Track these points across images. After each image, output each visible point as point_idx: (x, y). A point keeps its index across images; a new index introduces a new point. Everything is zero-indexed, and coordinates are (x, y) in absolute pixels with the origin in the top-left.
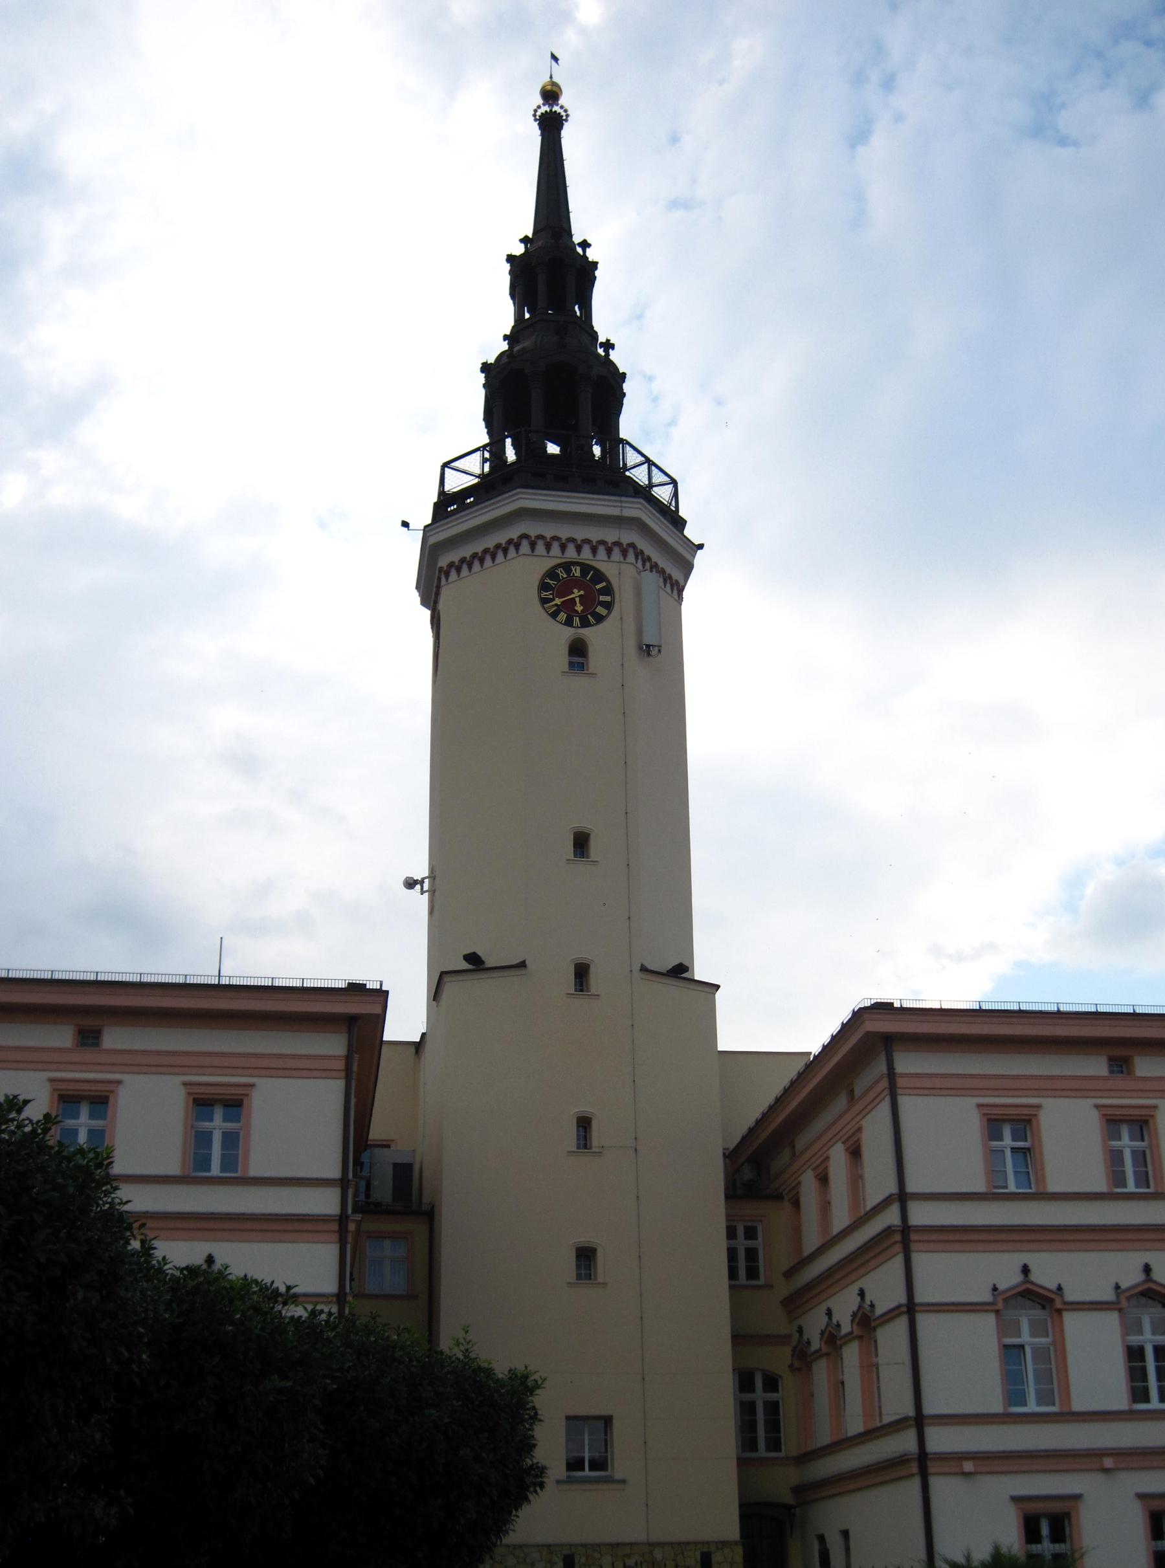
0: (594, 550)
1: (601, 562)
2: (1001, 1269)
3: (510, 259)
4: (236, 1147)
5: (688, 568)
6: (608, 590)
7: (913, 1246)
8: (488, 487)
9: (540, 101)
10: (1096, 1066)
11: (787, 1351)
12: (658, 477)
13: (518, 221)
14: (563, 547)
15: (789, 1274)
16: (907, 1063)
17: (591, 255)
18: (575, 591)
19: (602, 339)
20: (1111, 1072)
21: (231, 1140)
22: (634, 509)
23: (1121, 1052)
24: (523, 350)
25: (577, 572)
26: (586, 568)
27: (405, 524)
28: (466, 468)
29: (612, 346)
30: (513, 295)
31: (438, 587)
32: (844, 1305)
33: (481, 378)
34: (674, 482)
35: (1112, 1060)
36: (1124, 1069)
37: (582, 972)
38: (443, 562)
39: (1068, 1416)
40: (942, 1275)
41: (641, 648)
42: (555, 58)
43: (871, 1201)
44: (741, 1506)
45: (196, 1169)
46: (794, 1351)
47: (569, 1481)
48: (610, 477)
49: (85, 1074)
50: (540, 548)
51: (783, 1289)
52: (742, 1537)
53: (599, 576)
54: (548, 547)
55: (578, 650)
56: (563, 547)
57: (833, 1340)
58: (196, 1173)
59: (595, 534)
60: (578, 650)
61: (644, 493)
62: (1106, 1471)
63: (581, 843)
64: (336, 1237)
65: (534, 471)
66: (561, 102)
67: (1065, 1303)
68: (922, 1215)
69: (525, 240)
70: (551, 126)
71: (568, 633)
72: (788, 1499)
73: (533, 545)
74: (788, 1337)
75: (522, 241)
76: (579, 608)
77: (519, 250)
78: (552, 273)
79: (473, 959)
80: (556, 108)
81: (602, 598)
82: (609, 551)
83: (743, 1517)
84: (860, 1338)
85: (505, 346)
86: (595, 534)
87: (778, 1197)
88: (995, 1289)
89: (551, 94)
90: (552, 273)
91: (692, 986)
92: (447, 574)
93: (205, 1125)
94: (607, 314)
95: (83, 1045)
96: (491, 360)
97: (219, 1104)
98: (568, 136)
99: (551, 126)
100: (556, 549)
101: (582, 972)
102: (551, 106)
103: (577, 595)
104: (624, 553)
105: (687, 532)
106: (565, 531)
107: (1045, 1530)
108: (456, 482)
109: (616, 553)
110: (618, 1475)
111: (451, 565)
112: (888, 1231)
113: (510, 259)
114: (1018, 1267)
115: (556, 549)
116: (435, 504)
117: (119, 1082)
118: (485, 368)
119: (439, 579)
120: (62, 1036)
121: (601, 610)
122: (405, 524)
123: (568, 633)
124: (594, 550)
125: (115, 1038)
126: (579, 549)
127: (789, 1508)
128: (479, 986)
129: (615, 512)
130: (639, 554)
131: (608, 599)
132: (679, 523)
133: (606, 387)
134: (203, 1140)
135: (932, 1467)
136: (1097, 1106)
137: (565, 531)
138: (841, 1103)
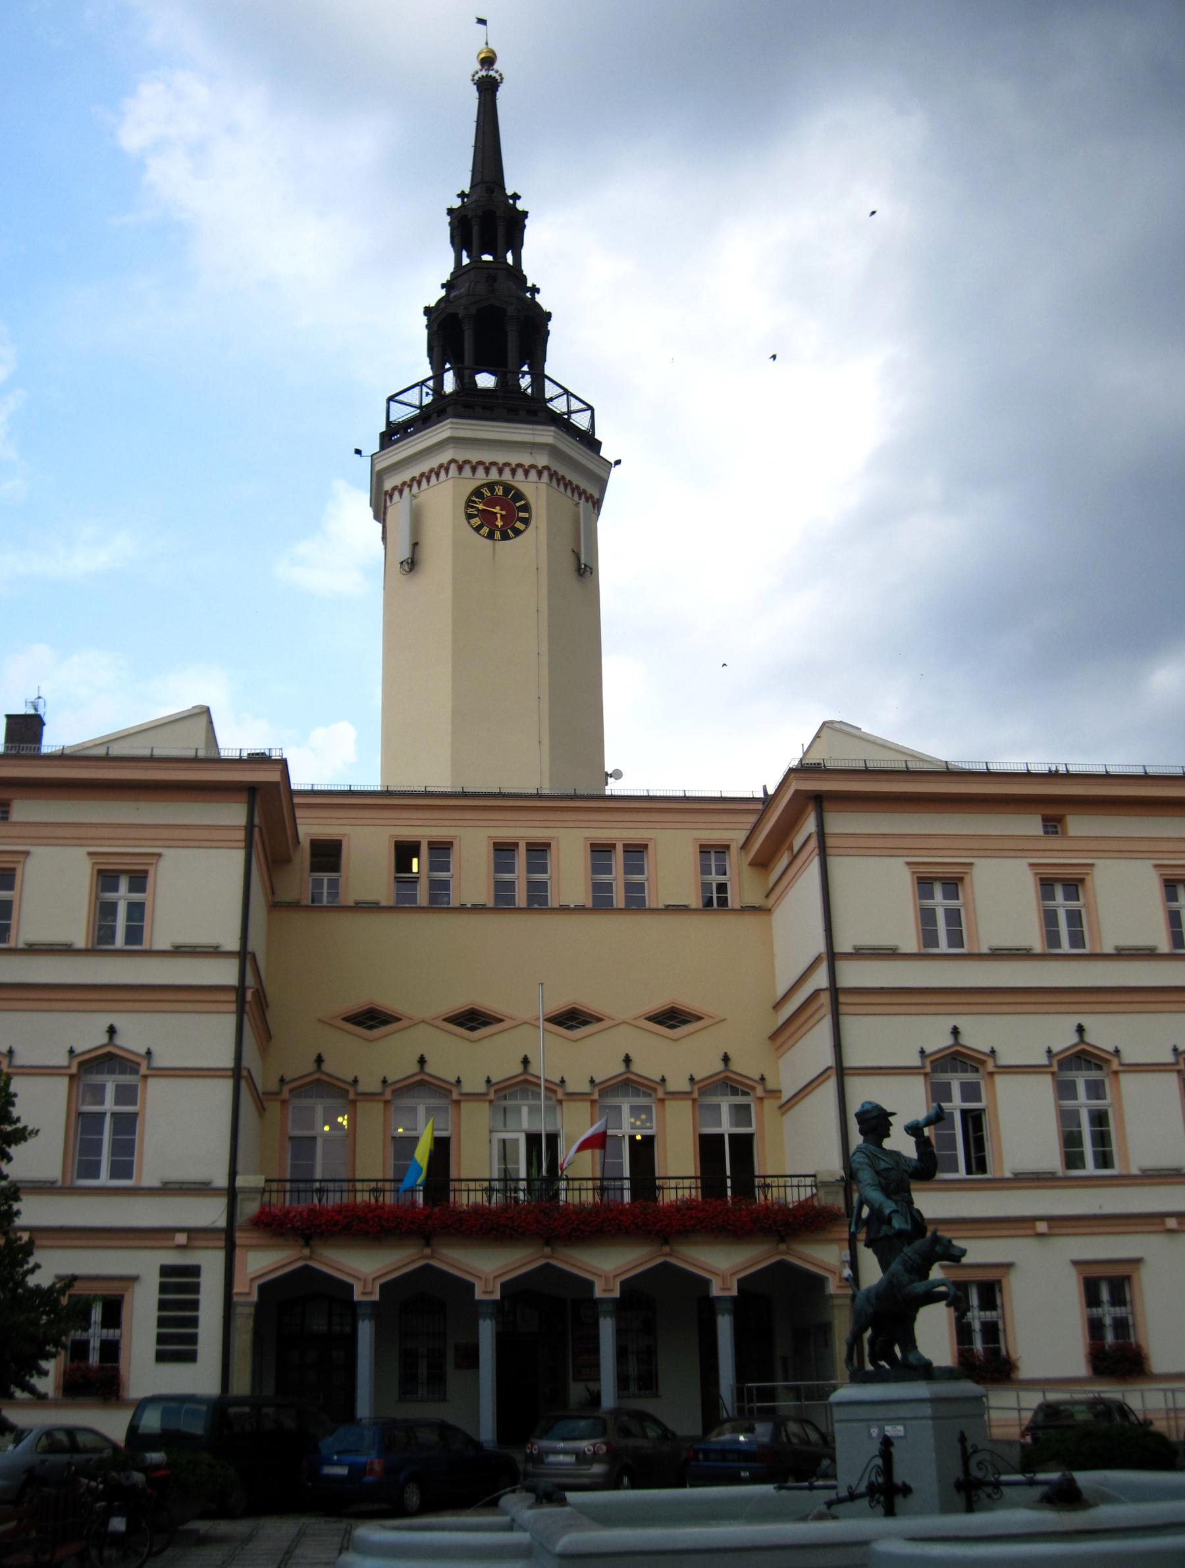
0: (513, 472)
2: (1058, 1032)
3: (450, 211)
4: (141, 918)
6: (526, 508)
7: (843, 1009)
8: (426, 418)
9: (479, 67)
10: (1030, 825)
13: (459, 178)
14: (487, 470)
16: (840, 823)
17: (520, 205)
18: (498, 508)
19: (529, 284)
20: (1046, 832)
21: (137, 911)
22: (547, 435)
24: (457, 298)
25: (499, 491)
26: (508, 488)
27: (358, 452)
28: (406, 400)
29: (538, 291)
31: (385, 507)
33: (424, 320)
34: (590, 408)
35: (1046, 820)
36: (1059, 829)
38: (388, 485)
39: (1001, 1183)
48: (534, 408)
50: (467, 470)
53: (519, 496)
54: (474, 469)
56: (487, 470)
58: (101, 942)
61: (562, 422)
62: (1170, 1231)
65: (469, 404)
66: (496, 67)
67: (1121, 1065)
68: (853, 975)
69: (462, 195)
70: (488, 88)
75: (459, 196)
76: (499, 523)
77: (457, 203)
78: (488, 222)
80: (492, 73)
81: (521, 515)
82: (526, 473)
85: (443, 293)
89: (488, 61)
90: (488, 222)
92: (391, 497)
93: (110, 896)
94: (543, 258)
96: (433, 305)
98: (503, 97)
99: (488, 88)
100: (480, 471)
102: (488, 70)
103: (497, 511)
105: (603, 453)
106: (487, 457)
107: (1105, 1295)
108: (401, 413)
111: (395, 488)
112: (816, 993)
113: (450, 211)
114: (949, 1028)
115: (480, 471)
116: (382, 435)
118: (428, 311)
121: (519, 525)
122: (358, 452)
124: (513, 472)
126: (501, 471)
131: (526, 515)
133: (531, 328)
134: (107, 910)
136: (908, 864)
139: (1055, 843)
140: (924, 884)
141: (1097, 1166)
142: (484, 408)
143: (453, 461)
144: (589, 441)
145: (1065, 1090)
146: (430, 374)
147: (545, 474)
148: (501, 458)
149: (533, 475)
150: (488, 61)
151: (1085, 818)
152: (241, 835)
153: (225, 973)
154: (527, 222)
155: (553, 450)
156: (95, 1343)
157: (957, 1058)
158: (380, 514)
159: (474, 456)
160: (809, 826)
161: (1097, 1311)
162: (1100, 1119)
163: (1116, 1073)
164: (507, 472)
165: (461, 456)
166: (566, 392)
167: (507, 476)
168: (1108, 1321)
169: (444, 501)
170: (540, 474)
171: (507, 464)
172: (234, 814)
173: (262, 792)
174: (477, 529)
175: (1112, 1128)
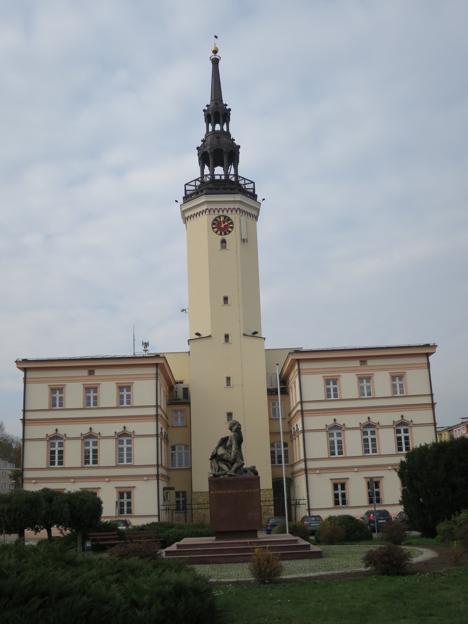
0: (227, 211)
1: (230, 215)
2: (328, 420)
3: (204, 111)
6: (232, 223)
7: (304, 415)
8: (198, 192)
10: (357, 363)
14: (218, 211)
16: (304, 366)
22: (238, 197)
26: (225, 217)
35: (361, 361)
37: (227, 337)
38: (186, 216)
39: (65, 468)
40: (313, 422)
44: (273, 479)
45: (120, 404)
49: (91, 382)
53: (229, 219)
54: (214, 212)
55: (224, 241)
56: (218, 211)
59: (227, 206)
60: (224, 241)
61: (244, 192)
63: (226, 299)
68: (307, 407)
69: (208, 106)
70: (215, 62)
71: (221, 237)
73: (210, 212)
75: (206, 106)
78: (218, 113)
79: (198, 334)
80: (217, 57)
81: (230, 226)
86: (227, 206)
88: (326, 425)
90: (218, 113)
91: (260, 339)
94: (238, 129)
97: (124, 388)
99: (215, 62)
101: (227, 337)
103: (222, 226)
106: (218, 206)
109: (234, 211)
111: (188, 217)
112: (298, 411)
113: (204, 111)
116: (184, 198)
118: (198, 148)
120: (85, 373)
121: (230, 229)
122: (176, 201)
123: (221, 237)
124: (227, 211)
125: (370, 363)
126: (223, 211)
129: (232, 199)
131: (232, 225)
135: (308, 472)
137: (218, 206)
139: (91, 377)
141: (373, 453)
143: (207, 209)
144: (253, 196)
146: (200, 176)
147: (238, 210)
148: (223, 206)
150: (215, 52)
151: (372, 360)
152: (155, 376)
153: (153, 412)
154: (231, 112)
155: (240, 202)
156: (125, 503)
157: (335, 427)
158: (185, 223)
159: (214, 206)
160: (296, 367)
161: (336, 492)
164: (225, 211)
165: (210, 207)
167: (225, 213)
169: (204, 222)
170: (236, 211)
172: (153, 371)
173: (157, 364)
174: (216, 232)
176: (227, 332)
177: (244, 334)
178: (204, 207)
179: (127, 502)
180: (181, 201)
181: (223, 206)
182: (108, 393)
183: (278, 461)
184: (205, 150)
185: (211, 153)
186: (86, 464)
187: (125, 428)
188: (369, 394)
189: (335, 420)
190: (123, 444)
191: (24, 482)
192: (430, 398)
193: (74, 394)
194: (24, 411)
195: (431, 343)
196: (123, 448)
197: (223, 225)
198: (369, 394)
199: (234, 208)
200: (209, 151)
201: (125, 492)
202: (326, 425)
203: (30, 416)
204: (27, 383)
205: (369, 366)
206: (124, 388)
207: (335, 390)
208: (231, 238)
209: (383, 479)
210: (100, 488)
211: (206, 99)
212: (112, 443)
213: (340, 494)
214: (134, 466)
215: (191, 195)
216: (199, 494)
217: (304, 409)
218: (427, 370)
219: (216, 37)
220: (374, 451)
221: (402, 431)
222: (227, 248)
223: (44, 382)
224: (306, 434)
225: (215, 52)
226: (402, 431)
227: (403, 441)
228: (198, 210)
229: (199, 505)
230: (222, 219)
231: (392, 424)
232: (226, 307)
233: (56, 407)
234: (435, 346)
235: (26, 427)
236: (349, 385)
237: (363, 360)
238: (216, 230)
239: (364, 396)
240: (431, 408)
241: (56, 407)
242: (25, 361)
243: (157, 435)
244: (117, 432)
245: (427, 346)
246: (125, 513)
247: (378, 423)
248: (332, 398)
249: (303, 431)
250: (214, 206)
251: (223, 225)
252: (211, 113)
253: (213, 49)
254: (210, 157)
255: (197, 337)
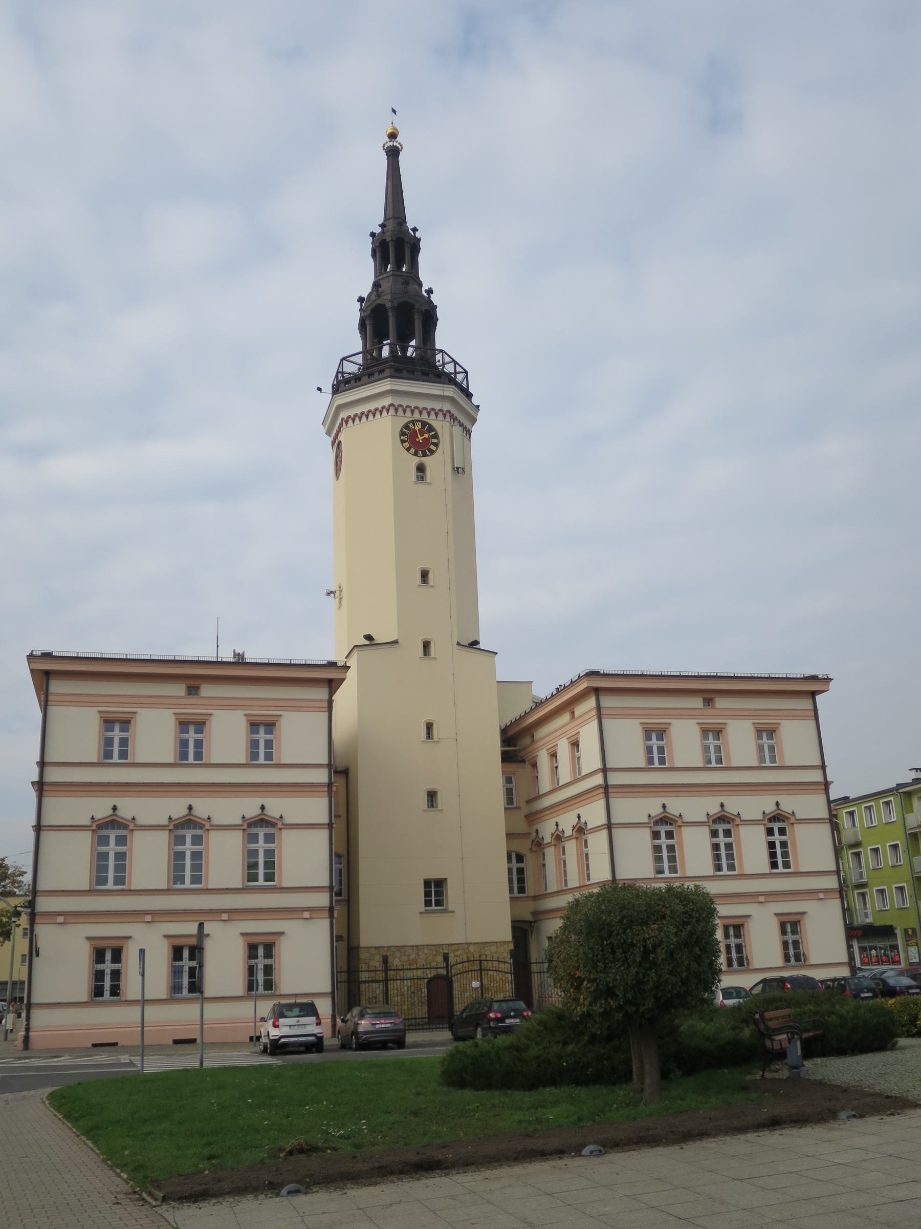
0: (429, 414)
3: (373, 235)
5: (473, 421)
6: (436, 436)
7: (610, 795)
10: (697, 703)
11: (529, 842)
12: (459, 369)
14: (412, 412)
15: (529, 802)
16: (608, 702)
17: (418, 235)
22: (450, 391)
23: (708, 696)
26: (424, 424)
30: (374, 255)
32: (567, 822)
34: (466, 372)
35: (704, 699)
37: (426, 645)
39: (743, 876)
41: (454, 469)
42: (394, 111)
43: (585, 772)
46: (533, 841)
47: (427, 912)
49: (192, 709)
51: (525, 810)
52: (513, 938)
53: (431, 429)
54: (404, 411)
55: (421, 469)
56: (412, 412)
57: (559, 838)
59: (429, 405)
60: (421, 469)
61: (450, 380)
63: (425, 575)
64: (326, 794)
68: (615, 779)
70: (393, 154)
72: (530, 918)
73: (396, 410)
74: (530, 834)
78: (396, 247)
79: (369, 637)
80: (395, 144)
81: (433, 441)
82: (437, 414)
83: (514, 928)
84: (577, 838)
86: (429, 405)
87: (523, 761)
88: (649, 816)
90: (396, 247)
94: (431, 272)
95: (189, 694)
97: (262, 726)
99: (393, 154)
101: (426, 645)
103: (418, 440)
104: (445, 416)
105: (473, 399)
106: (413, 403)
107: (789, 929)
110: (450, 909)
117: (211, 715)
119: (341, 424)
120: (179, 690)
122: (319, 389)
123: (416, 460)
124: (429, 414)
125: (207, 690)
126: (421, 413)
127: (530, 922)
128: (373, 654)
130: (452, 416)
131: (435, 441)
132: (469, 395)
137: (413, 403)
138: (565, 718)
139: (193, 700)
140: (254, 726)
141: (728, 870)
142: (408, 371)
143: (392, 405)
145: (656, 835)
148: (421, 404)
149: (441, 416)
150: (393, 136)
155: (452, 400)
156: (261, 966)
159: (405, 402)
161: (100, 967)
162: (270, 853)
163: (680, 826)
164: (416, 412)
166: (454, 361)
167: (425, 416)
168: (790, 941)
171: (408, 407)
174: (408, 450)
175: (275, 977)
176: (427, 637)
177: (458, 644)
178: (387, 402)
179: (112, 971)
180: (328, 389)
181: (421, 404)
182: (227, 735)
183: (519, 887)
184: (379, 301)
185: (392, 308)
186: (175, 883)
187: (263, 808)
188: (719, 760)
189: (664, 806)
190: (257, 843)
191: (37, 921)
192: (820, 772)
193: (154, 734)
194: (42, 764)
195: (820, 672)
196: (257, 851)
197: (420, 438)
198: (719, 760)
199: (441, 410)
200: (388, 305)
201: (108, 947)
202: (649, 816)
203: (54, 775)
204: (50, 703)
205: (718, 709)
206: (262, 726)
207: (661, 750)
208: (436, 463)
209: (282, 938)
210: (130, 937)
211: (374, 216)
212: (237, 838)
213: (733, 945)
214: (282, 888)
215: (347, 382)
216: (373, 951)
217: (610, 782)
218: (814, 722)
219: (394, 111)
220: (731, 867)
221: (663, 835)
222: (428, 480)
223: (90, 704)
224: (614, 831)
225: (393, 136)
226: (663, 835)
227: (778, 850)
228: (372, 406)
229: (373, 974)
230: (418, 427)
231: (760, 817)
232: (424, 589)
233: (112, 758)
234: (828, 680)
235: (46, 800)
236: (686, 742)
237: (709, 697)
238: (407, 445)
239: (710, 763)
240: (823, 792)
241: (112, 758)
242: (47, 656)
243: (330, 826)
244: (248, 816)
245: (814, 678)
246: (185, 991)
247: (739, 814)
248: (657, 765)
249: (609, 826)
250: (405, 402)
251: (420, 438)
252: (388, 239)
253: (390, 131)
254: (390, 314)
255: (367, 642)
